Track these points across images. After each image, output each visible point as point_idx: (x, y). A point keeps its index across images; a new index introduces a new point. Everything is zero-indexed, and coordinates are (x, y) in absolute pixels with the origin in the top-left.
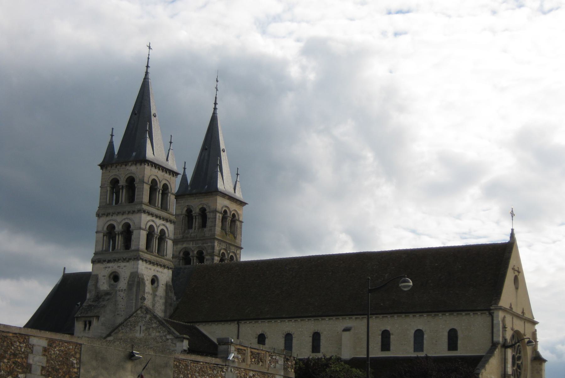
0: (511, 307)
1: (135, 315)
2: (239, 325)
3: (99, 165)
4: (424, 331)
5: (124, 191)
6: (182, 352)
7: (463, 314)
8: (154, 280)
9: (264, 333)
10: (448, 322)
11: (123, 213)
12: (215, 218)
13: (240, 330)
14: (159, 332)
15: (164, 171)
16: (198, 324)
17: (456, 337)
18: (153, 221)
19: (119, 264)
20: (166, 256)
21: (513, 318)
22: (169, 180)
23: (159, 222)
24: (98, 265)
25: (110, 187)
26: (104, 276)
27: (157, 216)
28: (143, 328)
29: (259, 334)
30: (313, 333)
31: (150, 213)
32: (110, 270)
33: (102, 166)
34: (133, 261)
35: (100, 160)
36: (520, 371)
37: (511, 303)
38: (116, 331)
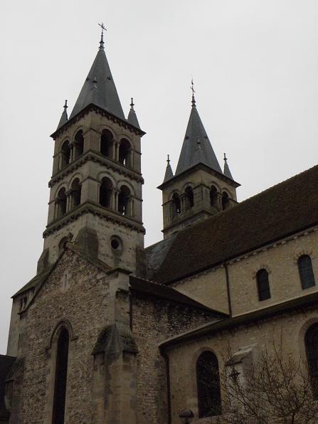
1: (60, 262)
2: (226, 268)
3: (51, 136)
6: (119, 295)
9: (265, 268)
12: (202, 192)
13: (229, 275)
14: (88, 274)
16: (174, 284)
19: (68, 227)
28: (69, 276)
29: (257, 271)
38: (39, 295)
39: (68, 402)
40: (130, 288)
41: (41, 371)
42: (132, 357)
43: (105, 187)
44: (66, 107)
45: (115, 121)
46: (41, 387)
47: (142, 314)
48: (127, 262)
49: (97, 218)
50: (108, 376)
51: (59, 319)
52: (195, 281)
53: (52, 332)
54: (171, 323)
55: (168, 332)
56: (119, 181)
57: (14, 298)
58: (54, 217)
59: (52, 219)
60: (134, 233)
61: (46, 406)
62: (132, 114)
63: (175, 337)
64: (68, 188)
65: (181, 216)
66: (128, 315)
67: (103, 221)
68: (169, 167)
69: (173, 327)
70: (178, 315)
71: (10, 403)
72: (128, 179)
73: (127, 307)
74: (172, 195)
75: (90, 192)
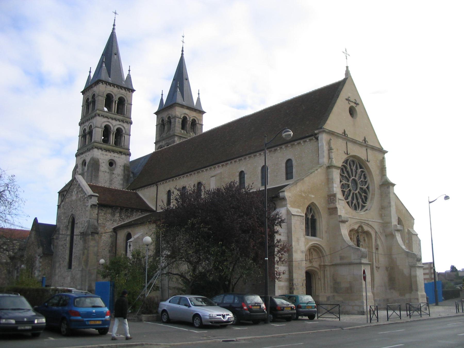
0: (365, 140)
3: (81, 92)
6: (92, 206)
7: (295, 144)
8: (111, 163)
9: (171, 190)
10: (285, 154)
15: (119, 88)
16: (137, 190)
17: (292, 166)
18: (109, 122)
21: (347, 143)
22: (125, 95)
23: (114, 122)
27: (112, 119)
28: (76, 192)
29: (168, 191)
30: (83, 159)
32: (82, 159)
33: (83, 92)
34: (92, 150)
35: (82, 90)
37: (365, 137)
39: (74, 250)
40: (97, 203)
41: (65, 233)
42: (96, 235)
43: (107, 131)
44: (90, 72)
45: (115, 86)
48: (118, 174)
49: (100, 151)
52: (146, 190)
53: (69, 218)
54: (121, 217)
55: (119, 221)
56: (115, 126)
57: (59, 193)
60: (123, 156)
61: (67, 251)
62: (129, 77)
63: (123, 223)
65: (164, 135)
66: (96, 215)
67: (104, 152)
68: (162, 100)
70: (125, 212)
71: (53, 248)
72: (121, 123)
73: (96, 212)
74: (161, 120)
75: (98, 135)
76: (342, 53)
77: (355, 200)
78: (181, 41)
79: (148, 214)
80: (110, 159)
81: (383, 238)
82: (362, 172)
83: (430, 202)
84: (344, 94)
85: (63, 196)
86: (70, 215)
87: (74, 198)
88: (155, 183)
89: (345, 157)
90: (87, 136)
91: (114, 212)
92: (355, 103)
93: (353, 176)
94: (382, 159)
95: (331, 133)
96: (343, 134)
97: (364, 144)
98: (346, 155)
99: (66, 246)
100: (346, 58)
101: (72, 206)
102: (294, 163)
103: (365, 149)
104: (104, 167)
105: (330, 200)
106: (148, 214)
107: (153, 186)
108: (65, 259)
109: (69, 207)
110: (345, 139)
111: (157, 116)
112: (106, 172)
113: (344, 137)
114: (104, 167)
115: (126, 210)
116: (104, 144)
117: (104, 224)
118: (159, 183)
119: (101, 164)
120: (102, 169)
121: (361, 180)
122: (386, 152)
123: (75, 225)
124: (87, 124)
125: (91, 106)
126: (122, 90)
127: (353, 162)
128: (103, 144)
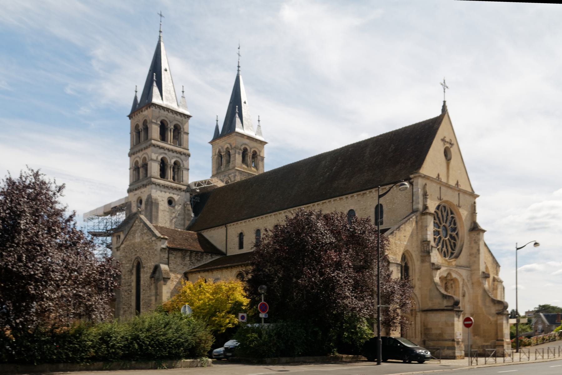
0: (457, 184)
4: (355, 210)
5: (143, 131)
9: (243, 232)
11: (142, 150)
14: (148, 236)
16: (203, 231)
18: (166, 154)
20: (183, 182)
22: (181, 121)
24: (132, 194)
25: (136, 132)
26: (134, 201)
31: (187, 154)
32: (137, 196)
33: (130, 117)
36: (454, 242)
39: (142, 296)
46: (129, 288)
47: (175, 258)
50: (156, 288)
51: (136, 256)
58: (133, 180)
59: (132, 181)
64: (140, 163)
66: (167, 260)
69: (192, 263)
72: (178, 155)
76: (440, 84)
77: (445, 246)
78: (158, 14)
79: (218, 257)
80: (169, 196)
81: (470, 286)
82: (453, 218)
83: (518, 249)
84: (441, 133)
85: (118, 237)
86: (134, 259)
87: (138, 240)
88: (225, 224)
89: (437, 203)
90: (141, 170)
91: (184, 255)
92: (450, 144)
93: (443, 222)
94: (473, 203)
95: (425, 177)
96: (437, 179)
97: (456, 188)
98: (439, 201)
99: (131, 291)
100: (443, 91)
101: (136, 249)
102: (385, 208)
103: (457, 193)
104: (163, 205)
105: (423, 247)
106: (218, 257)
107: (222, 228)
108: (131, 305)
109: (132, 250)
110: (439, 183)
111: (213, 146)
112: (165, 211)
113: (438, 182)
114: (163, 205)
115: (196, 253)
116: (162, 180)
117: (175, 269)
118: (228, 225)
119: (160, 203)
120: (161, 208)
121: (451, 226)
122: (478, 196)
123: (142, 270)
124: (140, 154)
125: (142, 134)
126: (177, 115)
127: (445, 207)
128: (160, 180)
